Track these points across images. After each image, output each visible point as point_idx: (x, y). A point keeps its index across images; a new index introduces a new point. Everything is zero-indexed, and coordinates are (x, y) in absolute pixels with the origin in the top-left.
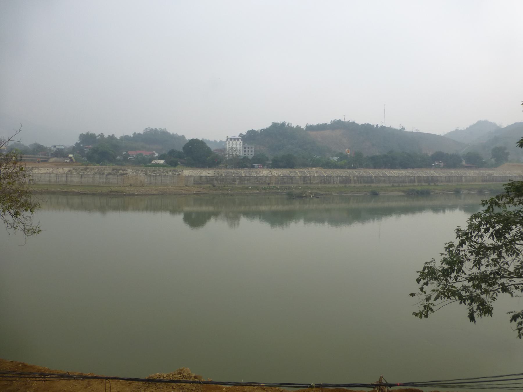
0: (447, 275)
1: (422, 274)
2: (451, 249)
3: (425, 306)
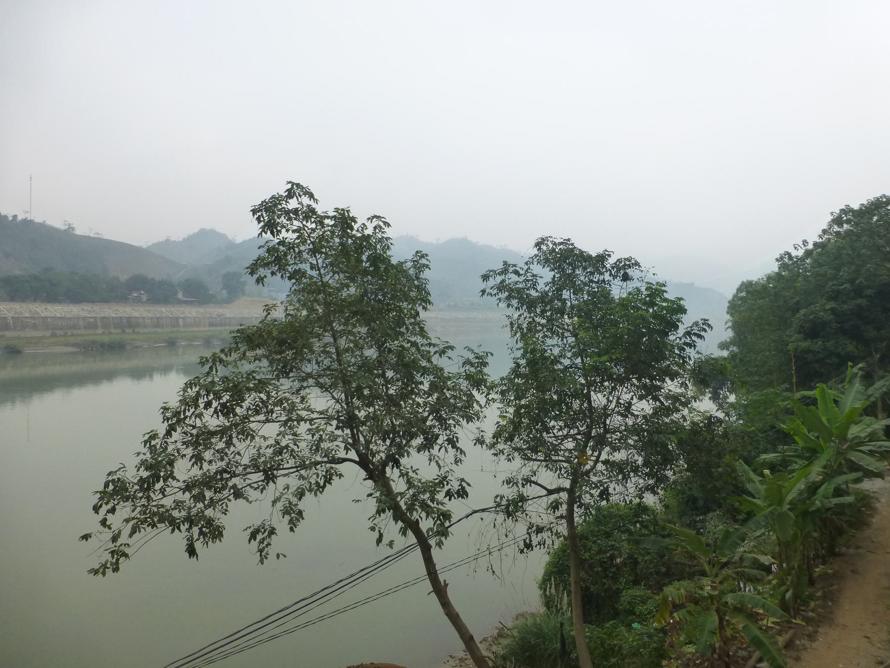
0: (148, 489)
1: (105, 496)
2: (153, 443)
3: (112, 553)
